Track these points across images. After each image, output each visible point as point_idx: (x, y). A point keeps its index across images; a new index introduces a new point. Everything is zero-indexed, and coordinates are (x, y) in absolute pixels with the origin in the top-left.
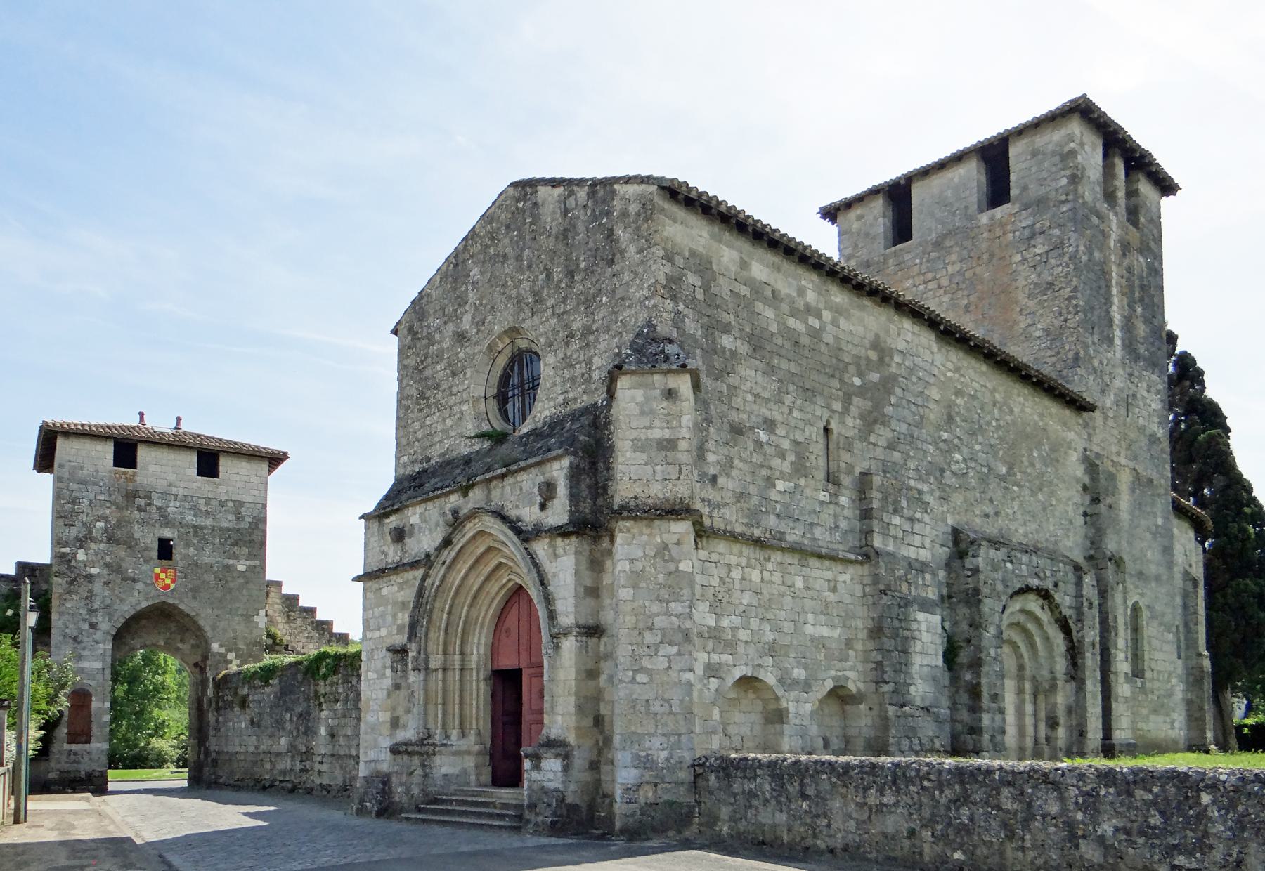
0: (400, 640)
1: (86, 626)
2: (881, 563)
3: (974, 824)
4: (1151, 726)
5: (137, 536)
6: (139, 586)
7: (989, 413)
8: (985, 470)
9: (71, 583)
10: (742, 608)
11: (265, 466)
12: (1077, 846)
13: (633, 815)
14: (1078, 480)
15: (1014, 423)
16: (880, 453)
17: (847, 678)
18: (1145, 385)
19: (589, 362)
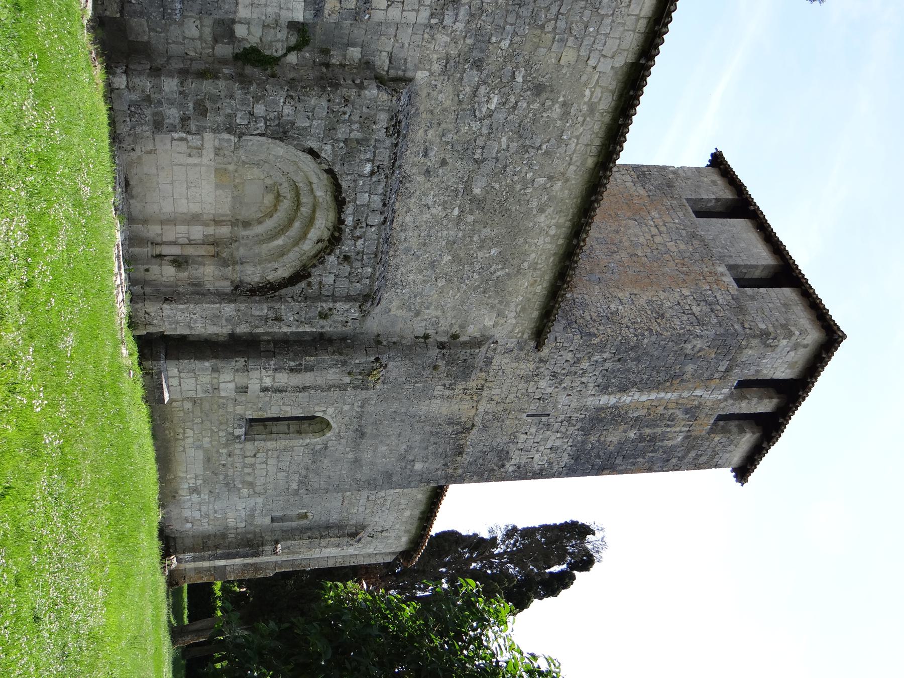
4: (190, 452)
14: (462, 327)
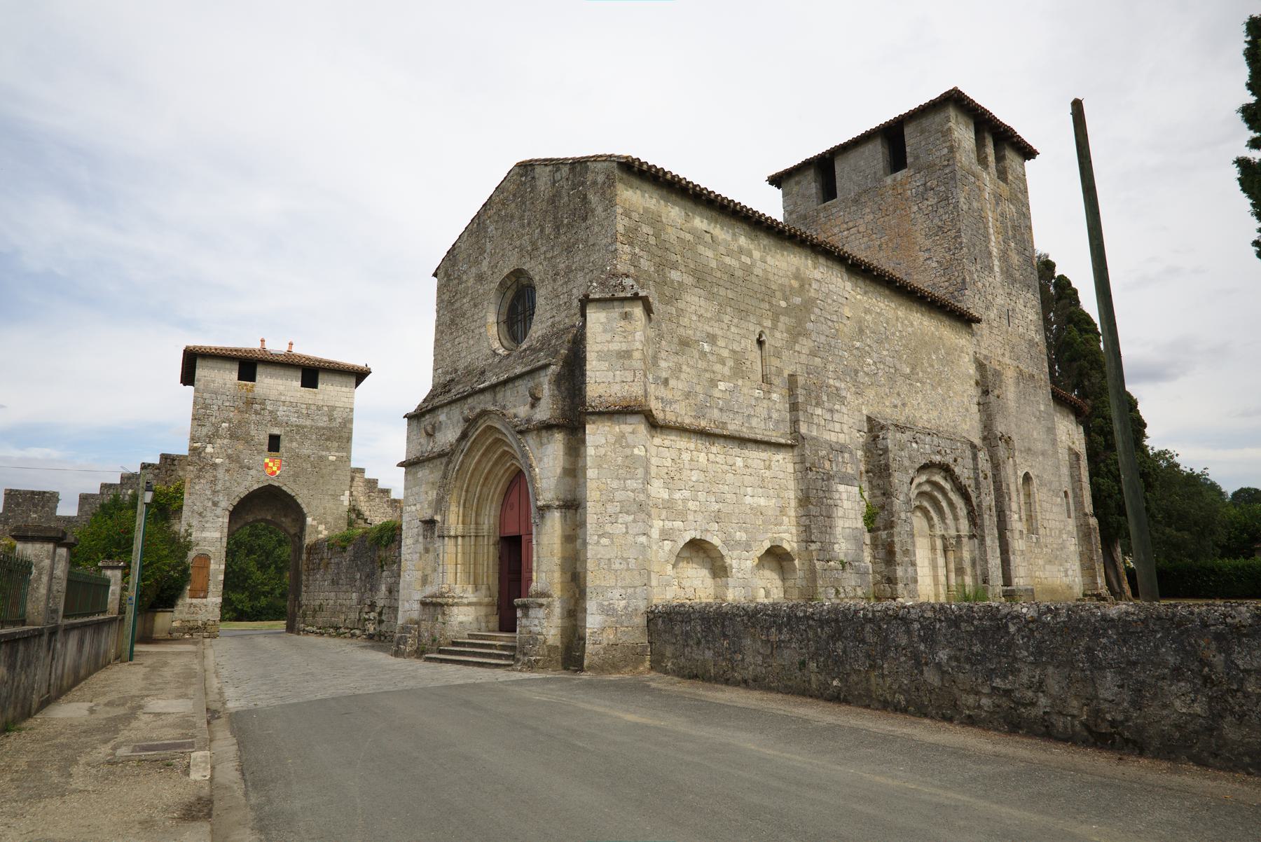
0: (428, 513)
1: (210, 504)
2: (807, 446)
3: (847, 655)
5: (253, 433)
6: (253, 472)
7: (894, 326)
8: (892, 370)
9: (200, 470)
10: (691, 484)
11: (354, 381)
12: (922, 672)
13: (597, 654)
14: (971, 377)
15: (914, 334)
16: (803, 359)
17: (782, 539)
18: (1021, 301)
19: (570, 293)
